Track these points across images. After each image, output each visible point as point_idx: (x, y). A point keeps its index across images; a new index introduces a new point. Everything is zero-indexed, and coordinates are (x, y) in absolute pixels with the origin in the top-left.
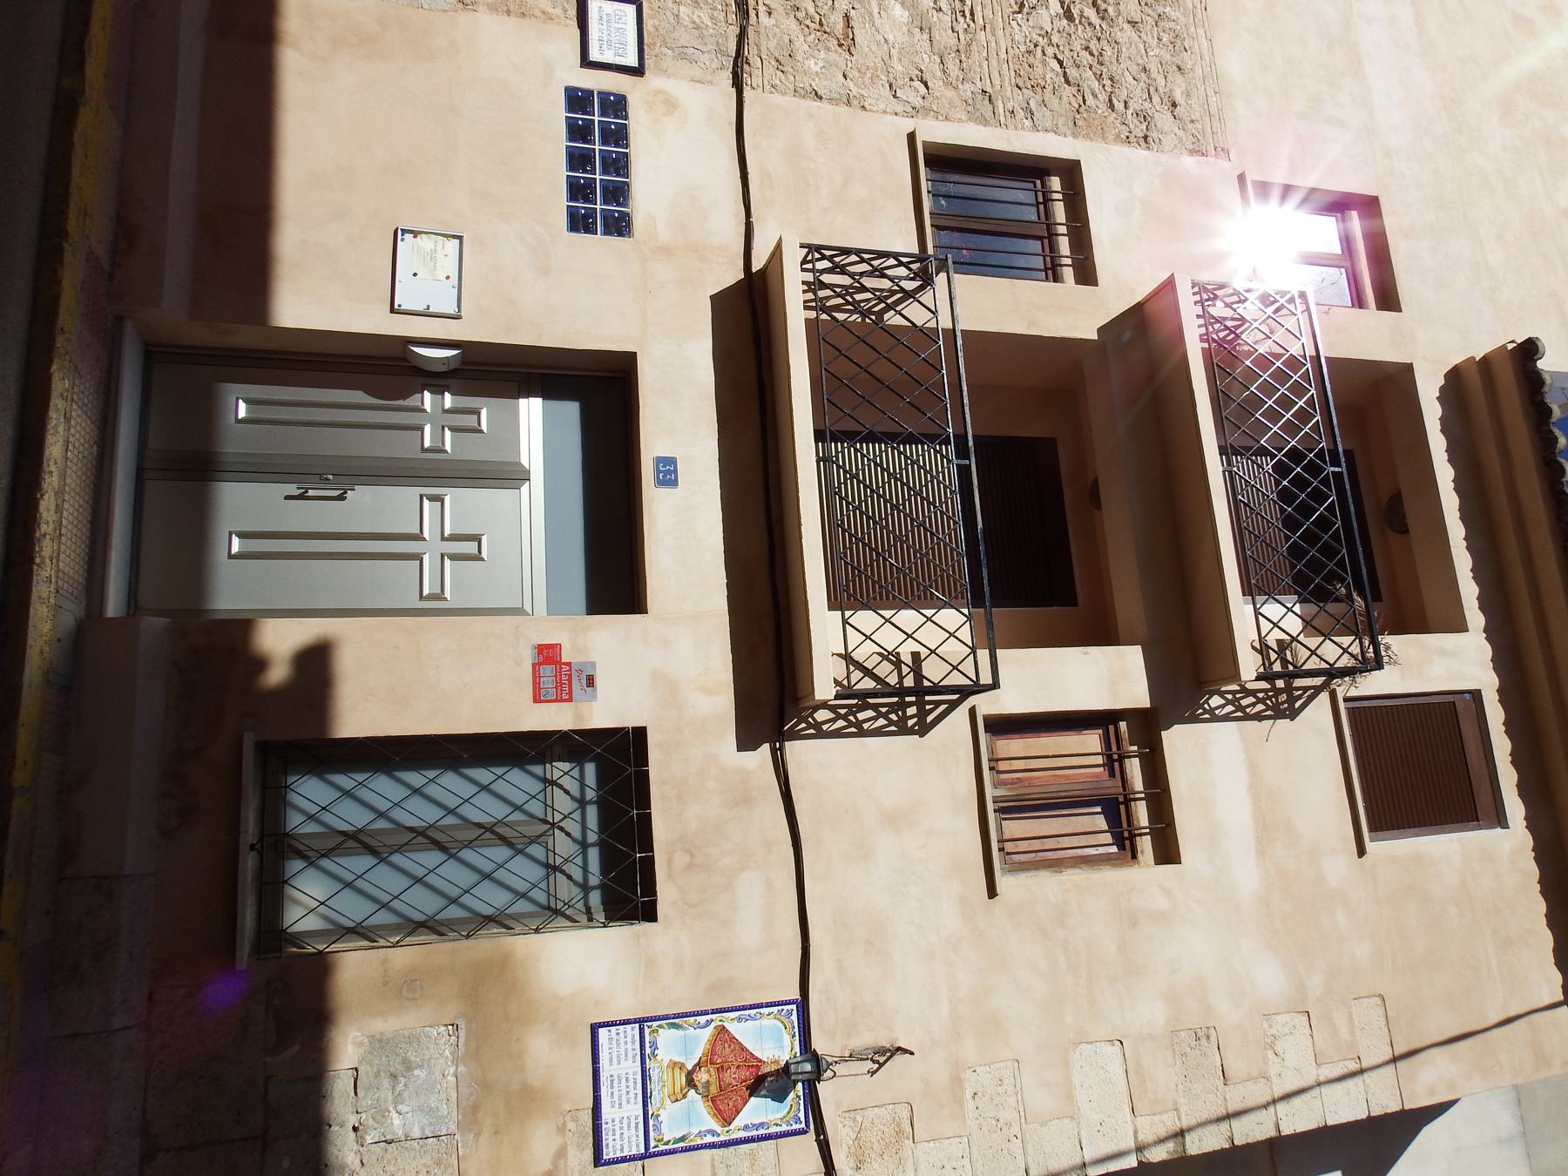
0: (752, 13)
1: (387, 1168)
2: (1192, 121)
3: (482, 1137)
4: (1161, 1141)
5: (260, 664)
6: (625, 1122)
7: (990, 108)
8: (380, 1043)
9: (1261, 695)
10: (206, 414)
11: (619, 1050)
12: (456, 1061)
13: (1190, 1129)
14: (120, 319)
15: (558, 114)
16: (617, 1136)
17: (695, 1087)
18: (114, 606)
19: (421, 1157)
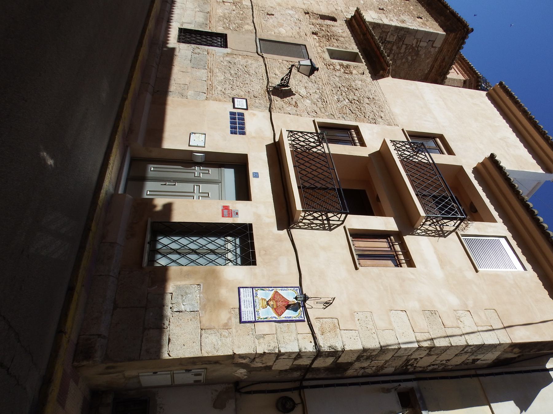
0: (273, 101)
1: (180, 318)
2: (387, 120)
3: (207, 312)
4: (425, 341)
5: (155, 206)
6: (249, 312)
7: (333, 117)
8: (178, 288)
9: (433, 231)
10: (145, 170)
11: (246, 295)
12: (200, 293)
13: (435, 339)
14: (127, 147)
15: (229, 116)
16: (246, 315)
17: (269, 305)
18: (121, 191)
19: (189, 316)
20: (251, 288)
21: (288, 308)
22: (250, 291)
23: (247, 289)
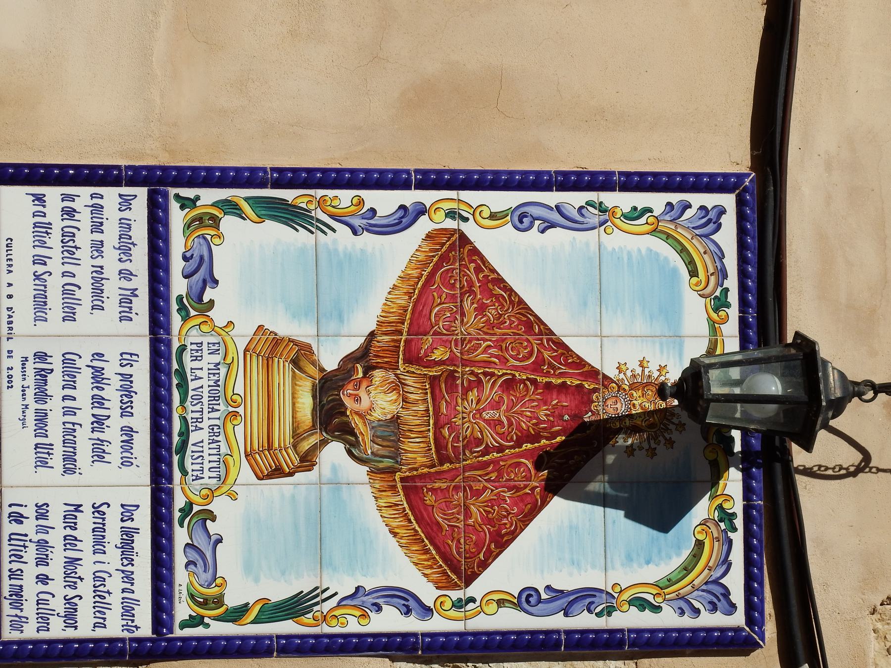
6: (86, 521)
16: (56, 569)
20: (132, 182)
21: (573, 472)
22: (126, 226)
23: (84, 193)
